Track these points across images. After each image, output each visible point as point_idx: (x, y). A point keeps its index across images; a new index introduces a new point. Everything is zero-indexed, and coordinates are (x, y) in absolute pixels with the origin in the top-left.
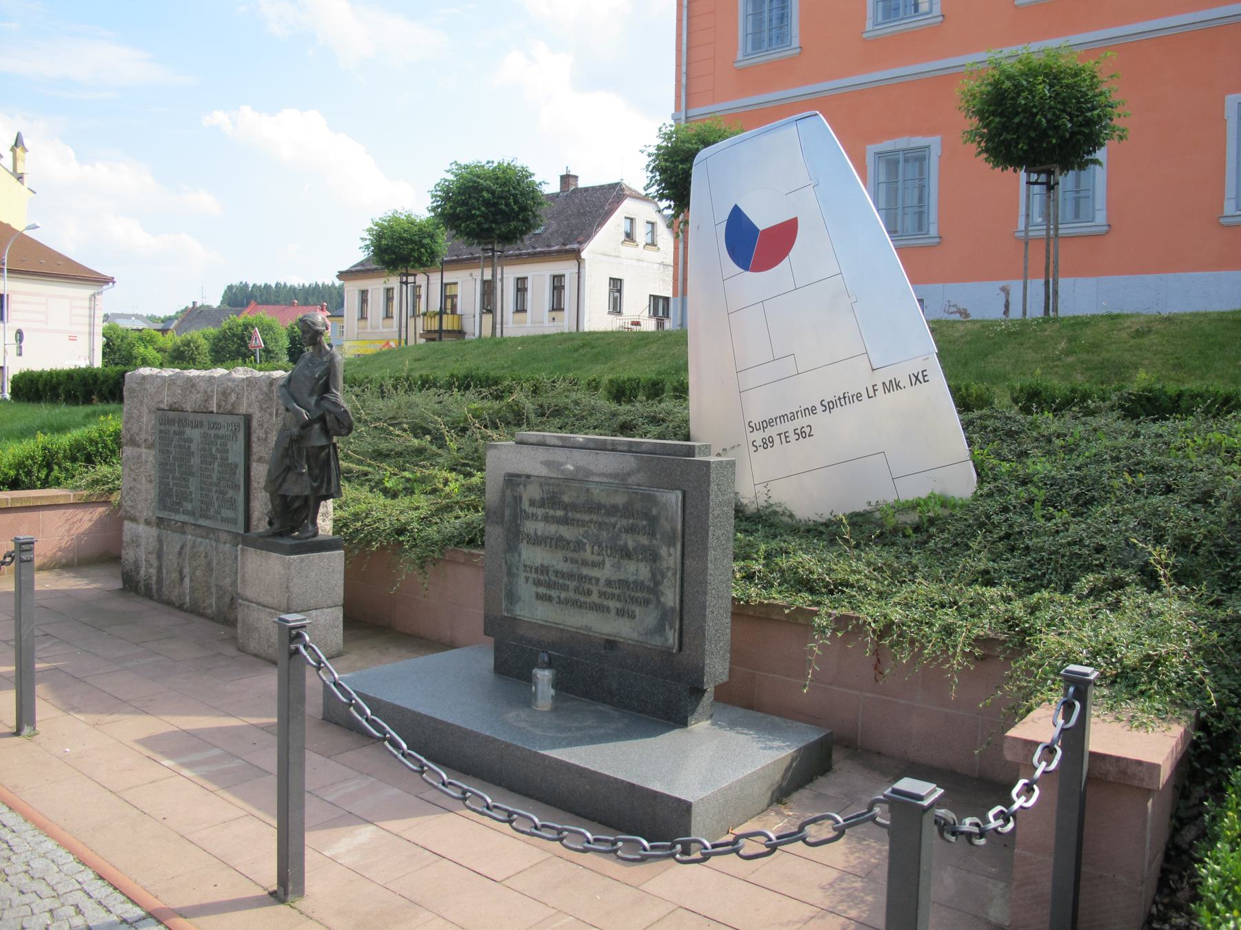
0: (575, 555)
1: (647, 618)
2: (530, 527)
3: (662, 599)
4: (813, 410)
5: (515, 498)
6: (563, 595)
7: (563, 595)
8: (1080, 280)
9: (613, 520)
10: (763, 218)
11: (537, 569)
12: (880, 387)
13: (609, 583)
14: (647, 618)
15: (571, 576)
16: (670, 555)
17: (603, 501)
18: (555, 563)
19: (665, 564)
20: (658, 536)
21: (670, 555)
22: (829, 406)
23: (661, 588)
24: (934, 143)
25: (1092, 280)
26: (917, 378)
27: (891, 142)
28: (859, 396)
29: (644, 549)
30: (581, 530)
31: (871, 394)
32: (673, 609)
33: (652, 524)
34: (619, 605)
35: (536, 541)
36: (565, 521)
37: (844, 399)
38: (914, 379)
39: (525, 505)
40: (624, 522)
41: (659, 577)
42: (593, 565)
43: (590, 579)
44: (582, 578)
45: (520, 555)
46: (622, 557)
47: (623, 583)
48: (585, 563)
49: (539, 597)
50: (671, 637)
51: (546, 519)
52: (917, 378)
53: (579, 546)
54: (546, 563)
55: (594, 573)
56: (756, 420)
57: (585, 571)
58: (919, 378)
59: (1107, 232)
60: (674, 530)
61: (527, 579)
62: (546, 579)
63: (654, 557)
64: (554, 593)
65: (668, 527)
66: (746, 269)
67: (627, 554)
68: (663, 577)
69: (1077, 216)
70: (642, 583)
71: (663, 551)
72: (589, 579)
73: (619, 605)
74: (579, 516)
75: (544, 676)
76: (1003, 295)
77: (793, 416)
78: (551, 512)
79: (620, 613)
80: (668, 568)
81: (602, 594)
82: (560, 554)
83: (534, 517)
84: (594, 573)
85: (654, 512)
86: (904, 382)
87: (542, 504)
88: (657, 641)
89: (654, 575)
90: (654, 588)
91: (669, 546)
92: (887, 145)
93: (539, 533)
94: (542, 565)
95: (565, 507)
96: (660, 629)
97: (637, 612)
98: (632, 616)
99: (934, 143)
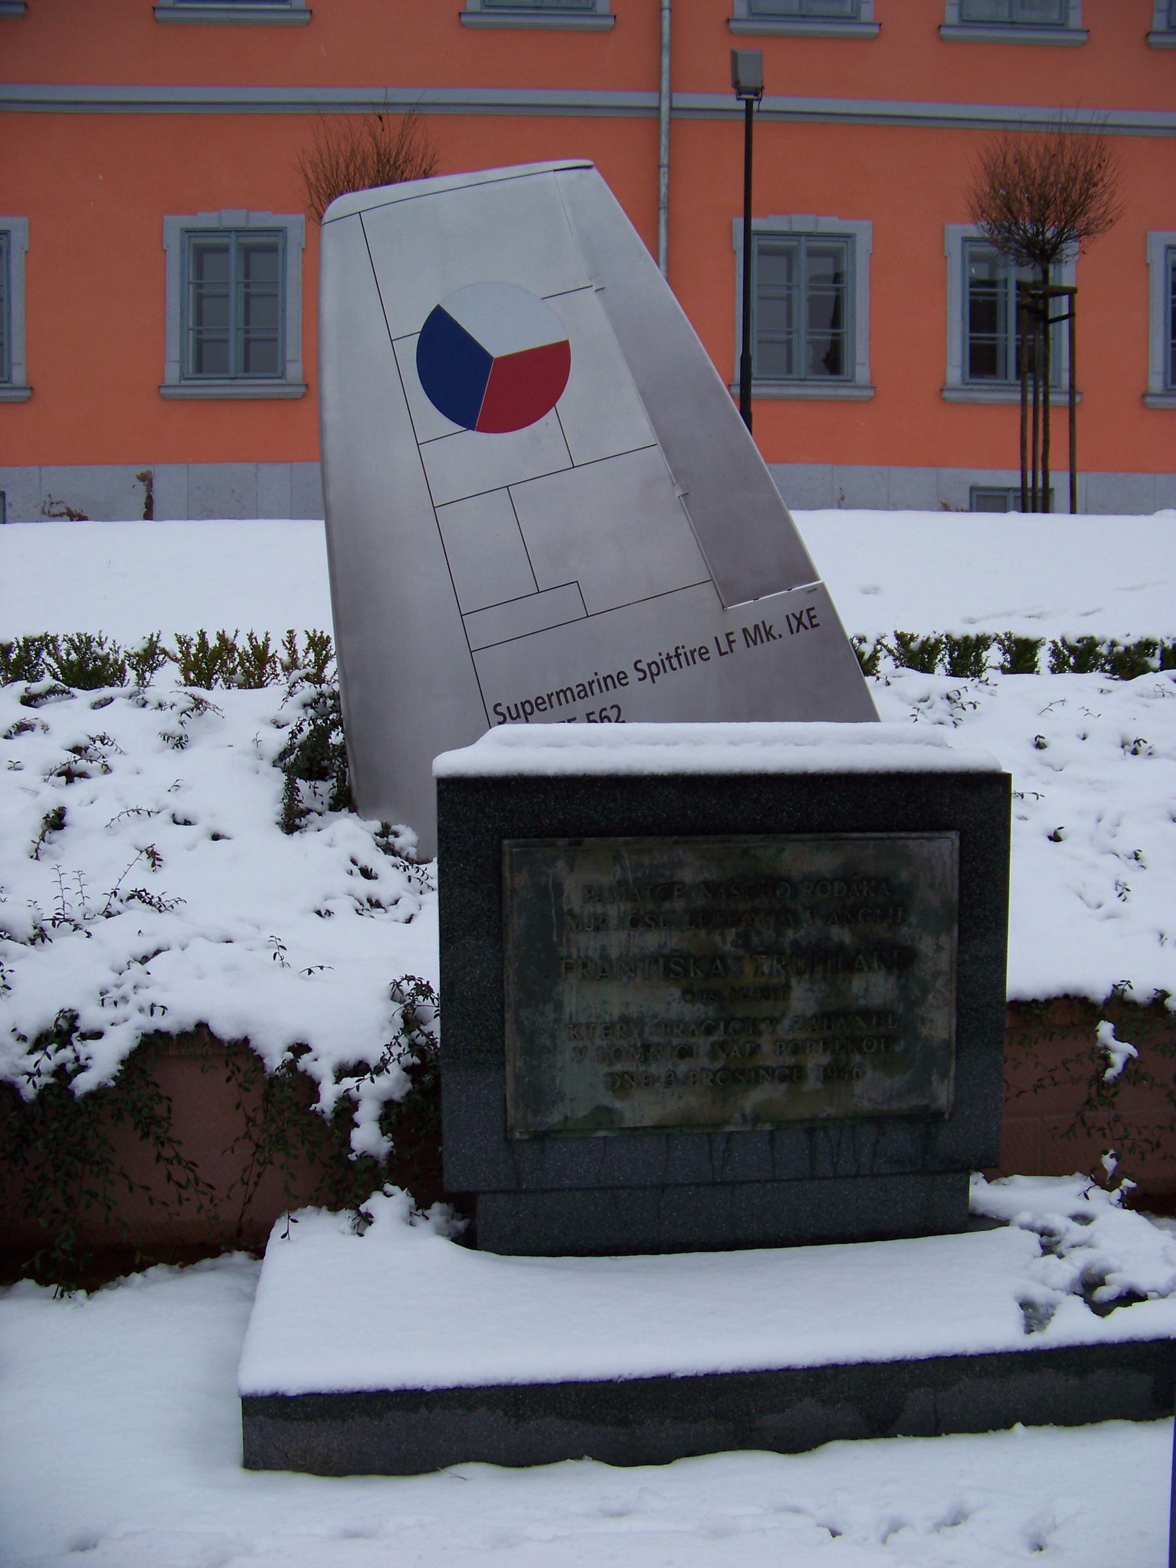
2: (587, 944)
4: (620, 679)
8: (265, 468)
10: (500, 335)
12: (738, 636)
16: (939, 948)
20: (913, 919)
24: (175, 224)
25: (283, 469)
27: (215, 215)
28: (703, 652)
35: (602, 970)
38: (794, 623)
39: (573, 899)
45: (559, 1007)
52: (799, 620)
54: (633, 1011)
59: (304, 395)
61: (581, 1052)
68: (925, 990)
69: (247, 370)
71: (926, 945)
76: (142, 487)
80: (936, 974)
83: (600, 924)
85: (904, 875)
86: (780, 627)
92: (206, 220)
93: (614, 953)
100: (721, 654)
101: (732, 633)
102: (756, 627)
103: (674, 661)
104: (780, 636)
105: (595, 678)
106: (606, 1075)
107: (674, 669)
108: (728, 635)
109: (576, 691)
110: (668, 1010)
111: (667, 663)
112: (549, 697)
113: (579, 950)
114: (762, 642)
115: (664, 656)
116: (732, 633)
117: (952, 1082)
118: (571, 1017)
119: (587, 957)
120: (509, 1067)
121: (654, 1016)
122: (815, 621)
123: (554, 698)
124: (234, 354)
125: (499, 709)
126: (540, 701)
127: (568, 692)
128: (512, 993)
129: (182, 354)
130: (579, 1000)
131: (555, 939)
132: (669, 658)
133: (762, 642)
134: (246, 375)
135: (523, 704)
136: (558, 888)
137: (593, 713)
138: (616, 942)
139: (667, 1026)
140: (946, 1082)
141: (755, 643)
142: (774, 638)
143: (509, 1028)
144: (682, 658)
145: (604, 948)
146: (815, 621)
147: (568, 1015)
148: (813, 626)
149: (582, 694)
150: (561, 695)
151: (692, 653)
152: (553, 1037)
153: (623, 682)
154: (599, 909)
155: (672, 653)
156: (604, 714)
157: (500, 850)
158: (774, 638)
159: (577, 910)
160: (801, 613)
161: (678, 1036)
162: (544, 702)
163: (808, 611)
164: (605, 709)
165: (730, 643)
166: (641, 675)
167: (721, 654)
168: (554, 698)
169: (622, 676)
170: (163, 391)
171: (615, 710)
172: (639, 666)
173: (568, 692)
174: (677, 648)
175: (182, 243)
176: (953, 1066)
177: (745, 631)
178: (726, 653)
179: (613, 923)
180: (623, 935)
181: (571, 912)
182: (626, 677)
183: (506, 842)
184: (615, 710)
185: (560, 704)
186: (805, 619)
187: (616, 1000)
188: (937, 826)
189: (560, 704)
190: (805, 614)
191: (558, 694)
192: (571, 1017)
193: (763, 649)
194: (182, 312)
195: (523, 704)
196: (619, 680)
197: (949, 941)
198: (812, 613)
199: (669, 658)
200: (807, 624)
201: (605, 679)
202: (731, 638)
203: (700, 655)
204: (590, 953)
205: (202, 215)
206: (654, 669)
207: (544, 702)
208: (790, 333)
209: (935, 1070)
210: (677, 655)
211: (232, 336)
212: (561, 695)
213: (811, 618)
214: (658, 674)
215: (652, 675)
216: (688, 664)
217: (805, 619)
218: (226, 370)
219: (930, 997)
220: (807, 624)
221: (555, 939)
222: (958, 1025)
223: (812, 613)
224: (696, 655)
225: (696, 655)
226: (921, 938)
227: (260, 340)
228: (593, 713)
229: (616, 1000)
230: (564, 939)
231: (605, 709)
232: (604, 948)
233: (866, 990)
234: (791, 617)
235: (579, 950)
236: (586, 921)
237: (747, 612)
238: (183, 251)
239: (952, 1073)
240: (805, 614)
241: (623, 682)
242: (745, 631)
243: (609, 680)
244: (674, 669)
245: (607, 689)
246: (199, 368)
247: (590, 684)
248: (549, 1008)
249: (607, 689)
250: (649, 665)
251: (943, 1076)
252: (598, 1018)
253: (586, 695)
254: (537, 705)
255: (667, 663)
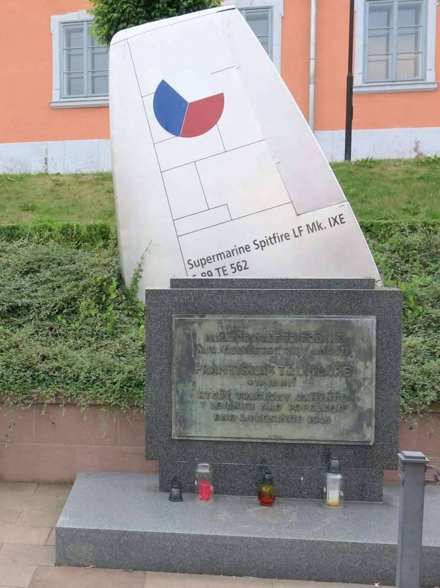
0: (263, 378)
1: (346, 421)
2: (206, 359)
3: (359, 404)
4: (247, 248)
5: (188, 336)
6: (247, 414)
7: (247, 414)
9: (305, 345)
10: (191, 91)
11: (216, 394)
12: (304, 228)
13: (301, 397)
14: (346, 421)
15: (259, 396)
16: (366, 367)
17: (293, 330)
18: (238, 387)
19: (361, 376)
20: (354, 354)
21: (366, 367)
22: (261, 245)
23: (358, 395)
24: (56, 20)
26: (335, 220)
27: (76, 13)
28: (287, 236)
29: (339, 366)
30: (268, 357)
31: (297, 233)
32: (370, 411)
33: (347, 345)
34: (312, 414)
35: (214, 371)
36: (249, 351)
37: (274, 239)
38: (332, 222)
39: (201, 340)
40: (317, 346)
41: (355, 387)
42: (284, 384)
43: (280, 396)
44: (270, 396)
45: (194, 383)
46: (316, 375)
47: (317, 396)
48: (274, 384)
49: (217, 418)
50: (369, 434)
51: (226, 350)
52: (335, 220)
53: (266, 369)
54: (226, 388)
55: (285, 390)
56: (194, 258)
57: (273, 390)
58: (337, 220)
60: (370, 348)
61: (204, 404)
62: (225, 403)
63: (351, 370)
64: (235, 413)
65: (364, 346)
66: (176, 133)
67: (320, 372)
68: (360, 385)
69: (93, 92)
70: (338, 393)
71: (360, 365)
72: (279, 397)
73: (312, 414)
74: (267, 345)
75: (334, 479)
77: (230, 254)
78: (233, 344)
79: (312, 421)
81: (292, 408)
82: (244, 380)
83: (212, 351)
84: (285, 390)
85: (349, 334)
86: (325, 224)
87: (222, 337)
88: (355, 438)
89: (350, 385)
90: (351, 395)
91: (365, 361)
93: (218, 363)
94: (222, 391)
95: (250, 339)
96: (358, 427)
97: (333, 419)
98: (327, 421)
99: (56, 20)
100: (296, 237)
101: (301, 227)
102: (313, 224)
103: (273, 240)
104: (325, 228)
105: (235, 248)
106: (214, 414)
107: (272, 244)
108: (299, 228)
109: (226, 254)
110: (241, 388)
111: (269, 241)
112: (213, 257)
113: (203, 361)
114: (316, 231)
115: (268, 238)
116: (301, 227)
117: (374, 428)
118: (199, 389)
119: (206, 364)
120: (173, 408)
121: (235, 390)
122: (343, 221)
123: (216, 257)
124: (86, 84)
125: (190, 262)
126: (209, 258)
127: (222, 255)
128: (175, 378)
129: (60, 85)
130: (203, 383)
131: (193, 356)
132: (270, 238)
133: (316, 231)
134: (93, 95)
135: (201, 260)
136: (194, 335)
137: (233, 264)
138: (219, 359)
139: (241, 395)
140: (370, 428)
141: (312, 231)
142: (322, 229)
143: (173, 392)
144: (277, 239)
145: (214, 360)
146: (343, 221)
147: (198, 388)
148: (342, 223)
149: (229, 255)
150: (219, 256)
151: (281, 236)
152: (191, 396)
153: (248, 250)
154: (212, 344)
155: (272, 236)
156: (239, 264)
157: (171, 319)
158: (322, 229)
159: (202, 344)
160: (336, 217)
161: (245, 399)
162: (211, 259)
163: (340, 216)
164: (239, 262)
165: (300, 231)
166: (257, 247)
167: (296, 237)
168: (216, 257)
169: (247, 247)
170: (51, 105)
171: (244, 263)
172: (256, 242)
173: (222, 255)
174: (274, 234)
175: (60, 29)
176: (374, 421)
177: (307, 225)
178: (297, 236)
179: (218, 351)
180: (222, 355)
181: (200, 345)
182: (249, 248)
183: (173, 315)
184: (244, 263)
185: (218, 260)
186: (338, 220)
187: (217, 383)
188: (366, 313)
189: (218, 260)
190: (338, 218)
191: (217, 255)
192: (199, 389)
193: (318, 234)
194: (60, 64)
195: (201, 260)
196: (246, 249)
197: (372, 364)
198: (342, 217)
199: (270, 238)
200: (339, 222)
201: (239, 249)
202: (301, 229)
203: (285, 237)
204: (208, 363)
205: (69, 14)
206: (263, 244)
207: (211, 259)
208: (416, 53)
209: (365, 422)
210: (274, 237)
211: (85, 75)
212: (219, 256)
213: (341, 219)
214: (265, 246)
215: (262, 246)
216: (279, 241)
217: (338, 220)
218: (82, 93)
219: (362, 389)
220: (339, 222)
221: (193, 356)
222: (376, 403)
223: (342, 217)
224: (283, 237)
225: (283, 237)
226: (357, 363)
227: (98, 76)
228: (233, 264)
229: (217, 383)
230: (197, 356)
231: (239, 262)
232: (214, 360)
233: (331, 383)
234: (331, 219)
235: (203, 361)
236: (206, 349)
237: (309, 218)
238: (60, 33)
239: (373, 424)
240: (338, 218)
241: (248, 250)
242: (307, 225)
243: (241, 249)
244: (272, 244)
245: (240, 253)
246: (69, 93)
247: (233, 251)
248: (191, 384)
249: (240, 253)
250: (261, 242)
251: (369, 425)
252: (211, 390)
253: (231, 256)
254: (208, 260)
255: (269, 241)
